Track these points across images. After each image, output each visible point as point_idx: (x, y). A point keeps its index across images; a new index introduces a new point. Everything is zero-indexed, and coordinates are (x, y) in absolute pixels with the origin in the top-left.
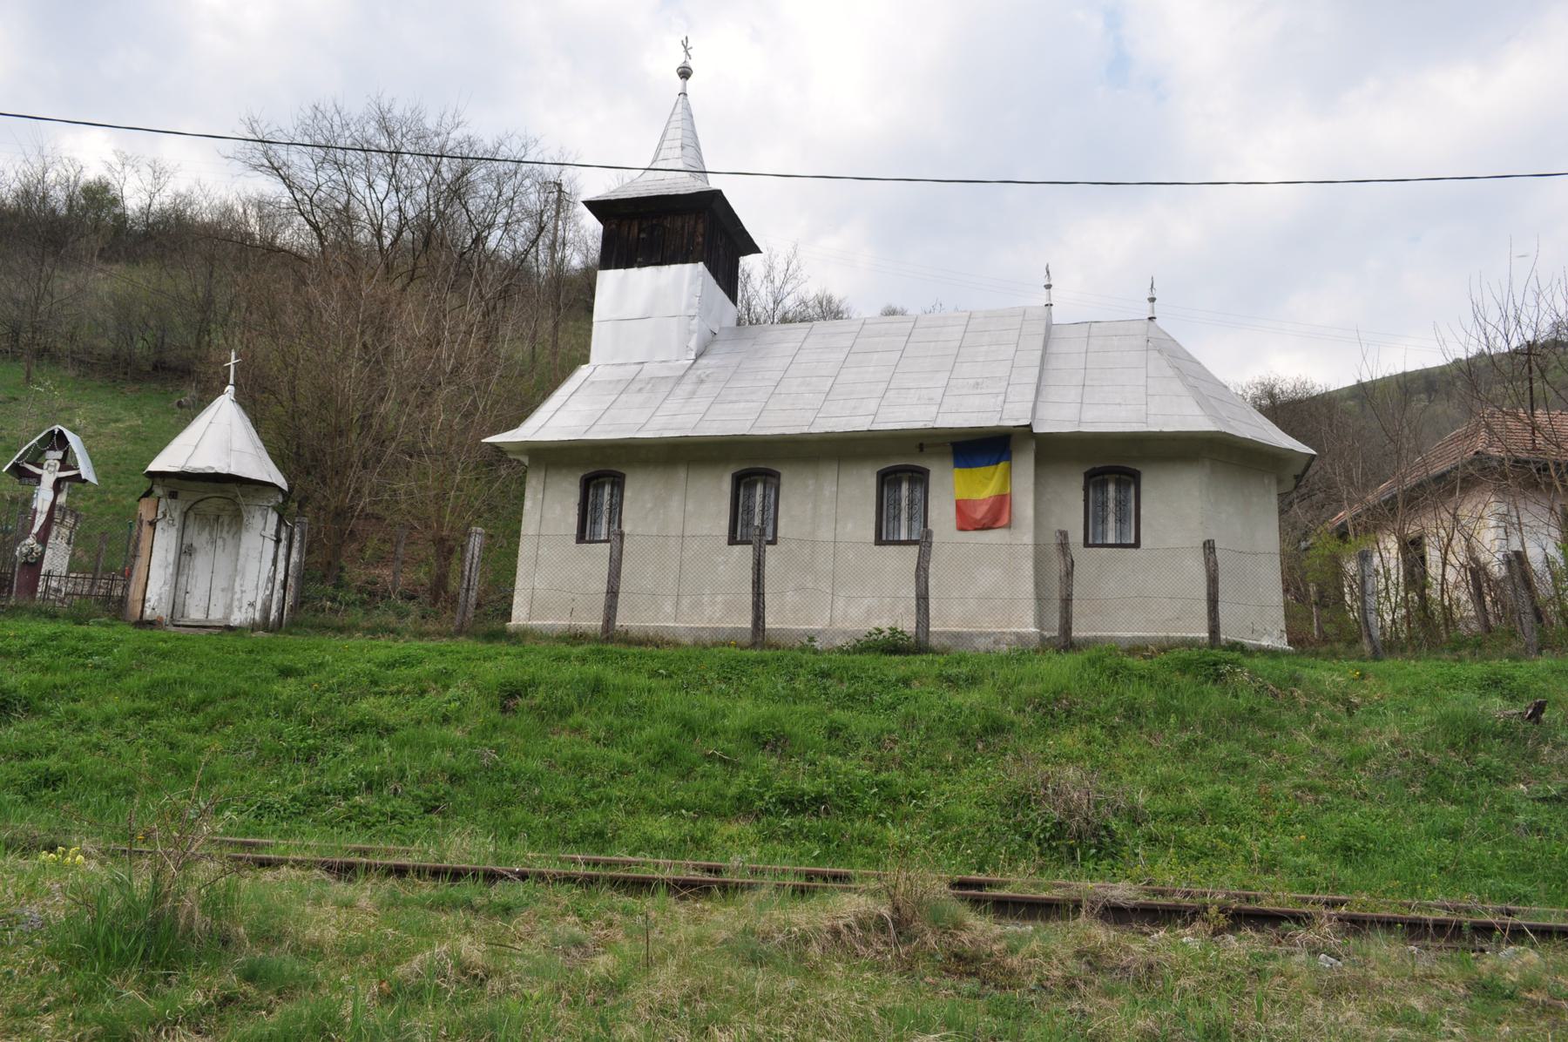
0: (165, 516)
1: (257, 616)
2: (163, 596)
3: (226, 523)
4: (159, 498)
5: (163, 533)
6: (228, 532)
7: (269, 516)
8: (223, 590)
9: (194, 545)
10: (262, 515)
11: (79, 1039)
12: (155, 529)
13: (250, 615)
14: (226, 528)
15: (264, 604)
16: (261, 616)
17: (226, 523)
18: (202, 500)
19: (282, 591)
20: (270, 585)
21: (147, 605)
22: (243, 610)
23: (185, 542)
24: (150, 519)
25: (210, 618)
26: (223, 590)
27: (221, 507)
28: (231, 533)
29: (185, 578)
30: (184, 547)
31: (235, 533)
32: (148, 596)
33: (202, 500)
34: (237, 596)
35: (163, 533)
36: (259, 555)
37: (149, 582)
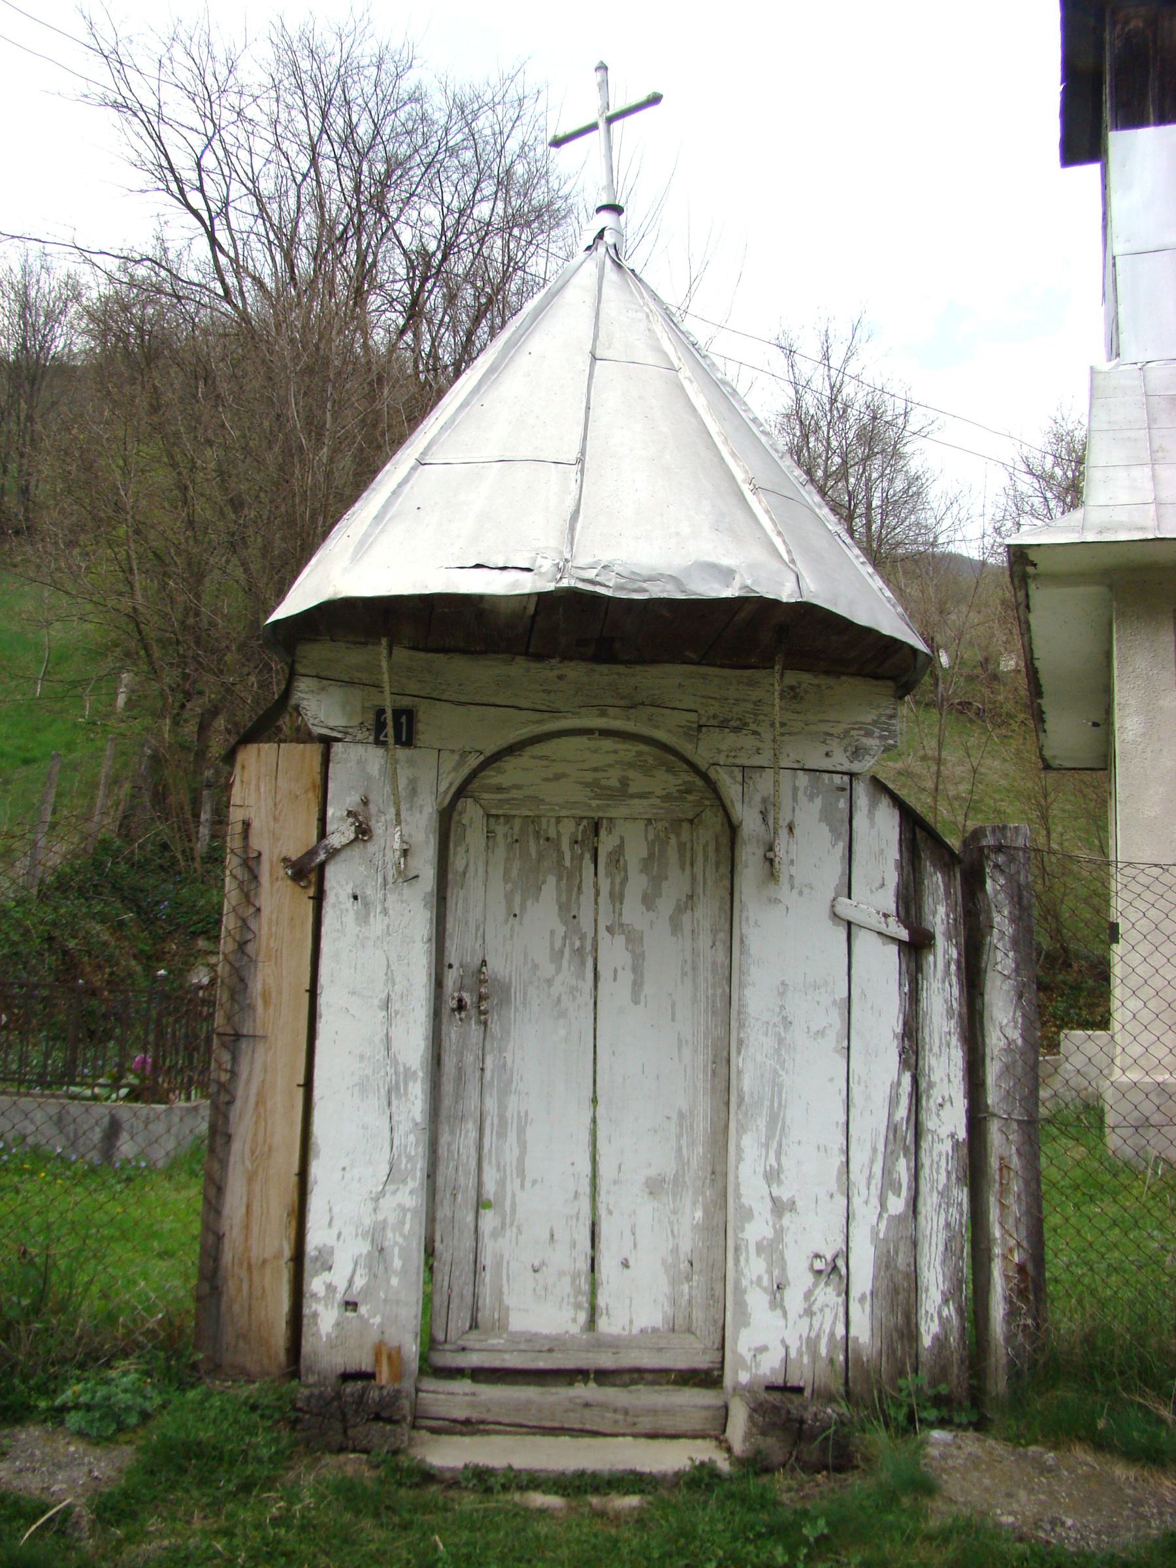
0: (363, 832)
1: (862, 1330)
2: (392, 1238)
3: (635, 853)
4: (327, 742)
5: (364, 919)
6: (648, 901)
7: (860, 821)
8: (654, 1187)
9: (497, 966)
10: (827, 816)
11: (3, 1245)
12: (319, 899)
13: (829, 1323)
14: (637, 883)
15: (885, 1264)
16: (877, 1326)
17: (635, 853)
18: (512, 750)
19: (962, 1195)
20: (902, 1167)
21: (316, 1284)
22: (794, 1299)
23: (452, 956)
24: (295, 852)
25: (604, 1325)
26: (654, 1187)
27: (612, 779)
28: (666, 905)
29: (471, 1126)
30: (451, 978)
31: (680, 909)
32: (315, 1238)
33: (512, 750)
34: (757, 1229)
35: (364, 919)
36: (836, 1020)
37: (317, 1169)
